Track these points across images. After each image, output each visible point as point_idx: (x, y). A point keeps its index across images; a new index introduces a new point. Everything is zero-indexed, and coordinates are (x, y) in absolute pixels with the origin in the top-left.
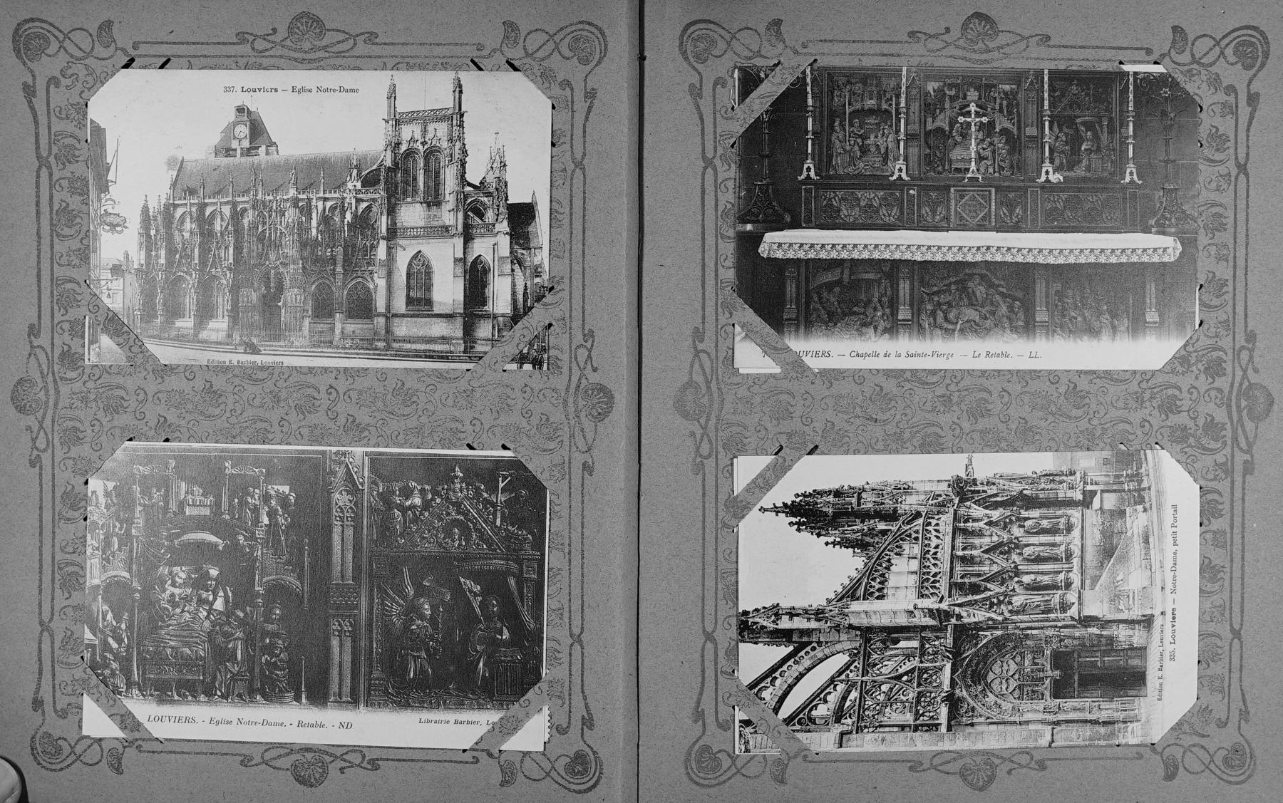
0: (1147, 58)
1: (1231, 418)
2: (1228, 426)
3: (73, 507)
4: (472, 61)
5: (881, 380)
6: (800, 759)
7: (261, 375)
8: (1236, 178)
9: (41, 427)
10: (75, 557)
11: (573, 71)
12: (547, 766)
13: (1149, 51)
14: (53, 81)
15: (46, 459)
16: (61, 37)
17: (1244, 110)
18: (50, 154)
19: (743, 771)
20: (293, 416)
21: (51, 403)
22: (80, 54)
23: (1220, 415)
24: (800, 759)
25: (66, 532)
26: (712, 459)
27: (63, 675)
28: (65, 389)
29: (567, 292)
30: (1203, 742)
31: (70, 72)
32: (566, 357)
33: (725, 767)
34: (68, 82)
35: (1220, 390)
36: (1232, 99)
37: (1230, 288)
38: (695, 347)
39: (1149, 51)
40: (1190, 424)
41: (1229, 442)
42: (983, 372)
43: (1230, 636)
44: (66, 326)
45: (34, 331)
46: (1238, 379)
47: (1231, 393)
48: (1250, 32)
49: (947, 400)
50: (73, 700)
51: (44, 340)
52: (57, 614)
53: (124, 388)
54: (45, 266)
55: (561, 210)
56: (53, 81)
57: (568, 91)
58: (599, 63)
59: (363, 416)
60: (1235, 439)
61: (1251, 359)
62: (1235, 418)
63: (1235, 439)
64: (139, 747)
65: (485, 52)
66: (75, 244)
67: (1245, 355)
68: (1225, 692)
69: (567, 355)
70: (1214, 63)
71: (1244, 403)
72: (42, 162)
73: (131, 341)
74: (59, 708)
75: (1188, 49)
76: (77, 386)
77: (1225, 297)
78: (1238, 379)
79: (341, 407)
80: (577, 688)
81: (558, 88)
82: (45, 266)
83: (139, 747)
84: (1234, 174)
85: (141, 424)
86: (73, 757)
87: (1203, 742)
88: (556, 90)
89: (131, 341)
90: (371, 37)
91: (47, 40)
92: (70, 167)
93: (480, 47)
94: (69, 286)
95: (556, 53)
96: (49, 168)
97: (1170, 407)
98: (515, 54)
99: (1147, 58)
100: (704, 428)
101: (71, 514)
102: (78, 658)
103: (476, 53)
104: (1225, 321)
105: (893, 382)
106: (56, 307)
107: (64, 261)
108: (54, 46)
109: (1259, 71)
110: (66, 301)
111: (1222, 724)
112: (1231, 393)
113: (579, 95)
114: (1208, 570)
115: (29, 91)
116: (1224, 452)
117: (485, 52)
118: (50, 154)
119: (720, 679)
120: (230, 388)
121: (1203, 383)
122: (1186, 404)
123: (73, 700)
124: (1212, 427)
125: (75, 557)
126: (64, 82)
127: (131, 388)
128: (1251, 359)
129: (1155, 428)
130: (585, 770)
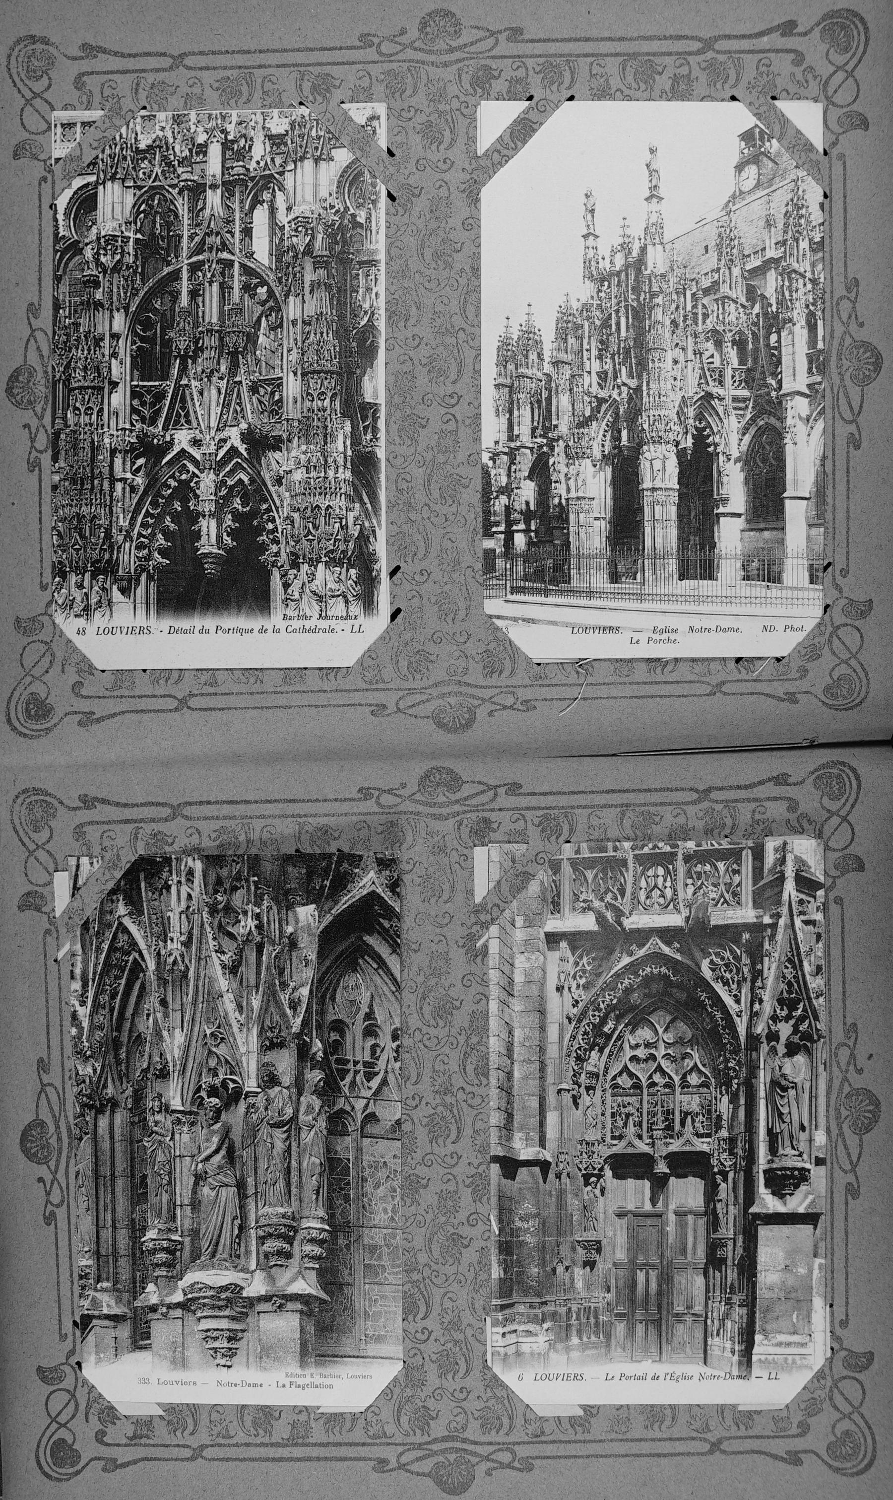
0: (837, 1322)
1: (435, 1441)
2: (426, 1438)
3: (315, 88)
4: (829, 564)
5: (467, 250)
6: (47, 926)
7: (471, 310)
8: (705, 1440)
9: (405, 46)
10: (258, 94)
11: (818, 1438)
12: (37, 672)
13: (844, 1324)
14: (799, 58)
15: (371, 54)
16: (849, 68)
17: (780, 1447)
18: (718, 52)
19: (28, 109)
20: (424, 351)
21: (432, 58)
22: (830, 92)
23: (438, 1429)
24: (47, 926)
25: (286, 80)
26: (376, 57)
27: (124, 83)
28: (449, 74)
29: (573, 1438)
30: (81, 1415)
31: (810, 77)
32: (500, 1438)
33: (34, 836)
34: (799, 77)
35: (464, 1428)
36: (794, 1430)
37: (580, 1437)
38: (500, 32)
39: (844, 1324)
40: (428, 1390)
41: (407, 685)
42: (477, 372)
43: (195, 1445)
44: (521, 73)
45: (514, 788)
46: (479, 1449)
47: (464, 1441)
48: (869, 1455)
49: (455, 1325)
50: (97, 98)
51: (505, 47)
52: (193, 73)
53: (451, 145)
54: (589, 47)
55: (663, 1427)
56: (799, 58)
57: (794, 1430)
58: (830, 1466)
59: (426, 437)
60: (411, 691)
61: (502, 1466)
62: (435, 1447)
63: (411, 691)
64: (44, 179)
65: (839, 578)
66: (615, 83)
67: (505, 1457)
68: (134, 1439)
69: (501, 1440)
70: (836, 1408)
71: (452, 1457)
72: (708, 44)
73: (505, 152)
74: (85, 78)
75: (849, 621)
76: (453, 89)
77: (571, 1431)
78: (479, 1449)
79: (437, 1172)
80: (124, 705)
81: (800, 1418)
82: (589, 47)
83: (44, 179)
84: (708, 1436)
85: (411, 166)
86: (29, 95)
87: (81, 1415)
88: (796, 1418)
89: (505, 152)
90: (855, 442)
91: (846, 50)
92: (703, 78)
93: (845, 573)
94: (567, 75)
95: (839, 1416)
96: (699, 52)
97: (447, 1365)
98: (836, 611)
99: (837, 1322)
100: (411, 45)
101: (307, 86)
102: (143, 103)
103: (838, 566)
104: (543, 1433)
105: (475, 1257)
106: (541, 813)
107: (595, 821)
108: (840, 59)
109: (826, 1463)
110: (551, 72)
111: (100, 1437)
112: (464, 1441)
113: (791, 687)
114: (266, 1415)
115: (788, 28)
116: (397, 1434)
117: (839, 578)
118: (718, 52)
119: (132, 826)
120: (454, 1031)
121: (473, 1405)
122: (451, 1384)
123: (97, 98)
124: (424, 1419)
125: (258, 94)
126: (798, 71)
127: (458, 1147)
128: (502, 1466)
129: (422, 1347)
130: (29, 716)
